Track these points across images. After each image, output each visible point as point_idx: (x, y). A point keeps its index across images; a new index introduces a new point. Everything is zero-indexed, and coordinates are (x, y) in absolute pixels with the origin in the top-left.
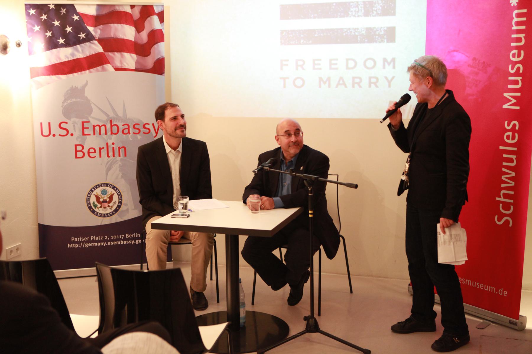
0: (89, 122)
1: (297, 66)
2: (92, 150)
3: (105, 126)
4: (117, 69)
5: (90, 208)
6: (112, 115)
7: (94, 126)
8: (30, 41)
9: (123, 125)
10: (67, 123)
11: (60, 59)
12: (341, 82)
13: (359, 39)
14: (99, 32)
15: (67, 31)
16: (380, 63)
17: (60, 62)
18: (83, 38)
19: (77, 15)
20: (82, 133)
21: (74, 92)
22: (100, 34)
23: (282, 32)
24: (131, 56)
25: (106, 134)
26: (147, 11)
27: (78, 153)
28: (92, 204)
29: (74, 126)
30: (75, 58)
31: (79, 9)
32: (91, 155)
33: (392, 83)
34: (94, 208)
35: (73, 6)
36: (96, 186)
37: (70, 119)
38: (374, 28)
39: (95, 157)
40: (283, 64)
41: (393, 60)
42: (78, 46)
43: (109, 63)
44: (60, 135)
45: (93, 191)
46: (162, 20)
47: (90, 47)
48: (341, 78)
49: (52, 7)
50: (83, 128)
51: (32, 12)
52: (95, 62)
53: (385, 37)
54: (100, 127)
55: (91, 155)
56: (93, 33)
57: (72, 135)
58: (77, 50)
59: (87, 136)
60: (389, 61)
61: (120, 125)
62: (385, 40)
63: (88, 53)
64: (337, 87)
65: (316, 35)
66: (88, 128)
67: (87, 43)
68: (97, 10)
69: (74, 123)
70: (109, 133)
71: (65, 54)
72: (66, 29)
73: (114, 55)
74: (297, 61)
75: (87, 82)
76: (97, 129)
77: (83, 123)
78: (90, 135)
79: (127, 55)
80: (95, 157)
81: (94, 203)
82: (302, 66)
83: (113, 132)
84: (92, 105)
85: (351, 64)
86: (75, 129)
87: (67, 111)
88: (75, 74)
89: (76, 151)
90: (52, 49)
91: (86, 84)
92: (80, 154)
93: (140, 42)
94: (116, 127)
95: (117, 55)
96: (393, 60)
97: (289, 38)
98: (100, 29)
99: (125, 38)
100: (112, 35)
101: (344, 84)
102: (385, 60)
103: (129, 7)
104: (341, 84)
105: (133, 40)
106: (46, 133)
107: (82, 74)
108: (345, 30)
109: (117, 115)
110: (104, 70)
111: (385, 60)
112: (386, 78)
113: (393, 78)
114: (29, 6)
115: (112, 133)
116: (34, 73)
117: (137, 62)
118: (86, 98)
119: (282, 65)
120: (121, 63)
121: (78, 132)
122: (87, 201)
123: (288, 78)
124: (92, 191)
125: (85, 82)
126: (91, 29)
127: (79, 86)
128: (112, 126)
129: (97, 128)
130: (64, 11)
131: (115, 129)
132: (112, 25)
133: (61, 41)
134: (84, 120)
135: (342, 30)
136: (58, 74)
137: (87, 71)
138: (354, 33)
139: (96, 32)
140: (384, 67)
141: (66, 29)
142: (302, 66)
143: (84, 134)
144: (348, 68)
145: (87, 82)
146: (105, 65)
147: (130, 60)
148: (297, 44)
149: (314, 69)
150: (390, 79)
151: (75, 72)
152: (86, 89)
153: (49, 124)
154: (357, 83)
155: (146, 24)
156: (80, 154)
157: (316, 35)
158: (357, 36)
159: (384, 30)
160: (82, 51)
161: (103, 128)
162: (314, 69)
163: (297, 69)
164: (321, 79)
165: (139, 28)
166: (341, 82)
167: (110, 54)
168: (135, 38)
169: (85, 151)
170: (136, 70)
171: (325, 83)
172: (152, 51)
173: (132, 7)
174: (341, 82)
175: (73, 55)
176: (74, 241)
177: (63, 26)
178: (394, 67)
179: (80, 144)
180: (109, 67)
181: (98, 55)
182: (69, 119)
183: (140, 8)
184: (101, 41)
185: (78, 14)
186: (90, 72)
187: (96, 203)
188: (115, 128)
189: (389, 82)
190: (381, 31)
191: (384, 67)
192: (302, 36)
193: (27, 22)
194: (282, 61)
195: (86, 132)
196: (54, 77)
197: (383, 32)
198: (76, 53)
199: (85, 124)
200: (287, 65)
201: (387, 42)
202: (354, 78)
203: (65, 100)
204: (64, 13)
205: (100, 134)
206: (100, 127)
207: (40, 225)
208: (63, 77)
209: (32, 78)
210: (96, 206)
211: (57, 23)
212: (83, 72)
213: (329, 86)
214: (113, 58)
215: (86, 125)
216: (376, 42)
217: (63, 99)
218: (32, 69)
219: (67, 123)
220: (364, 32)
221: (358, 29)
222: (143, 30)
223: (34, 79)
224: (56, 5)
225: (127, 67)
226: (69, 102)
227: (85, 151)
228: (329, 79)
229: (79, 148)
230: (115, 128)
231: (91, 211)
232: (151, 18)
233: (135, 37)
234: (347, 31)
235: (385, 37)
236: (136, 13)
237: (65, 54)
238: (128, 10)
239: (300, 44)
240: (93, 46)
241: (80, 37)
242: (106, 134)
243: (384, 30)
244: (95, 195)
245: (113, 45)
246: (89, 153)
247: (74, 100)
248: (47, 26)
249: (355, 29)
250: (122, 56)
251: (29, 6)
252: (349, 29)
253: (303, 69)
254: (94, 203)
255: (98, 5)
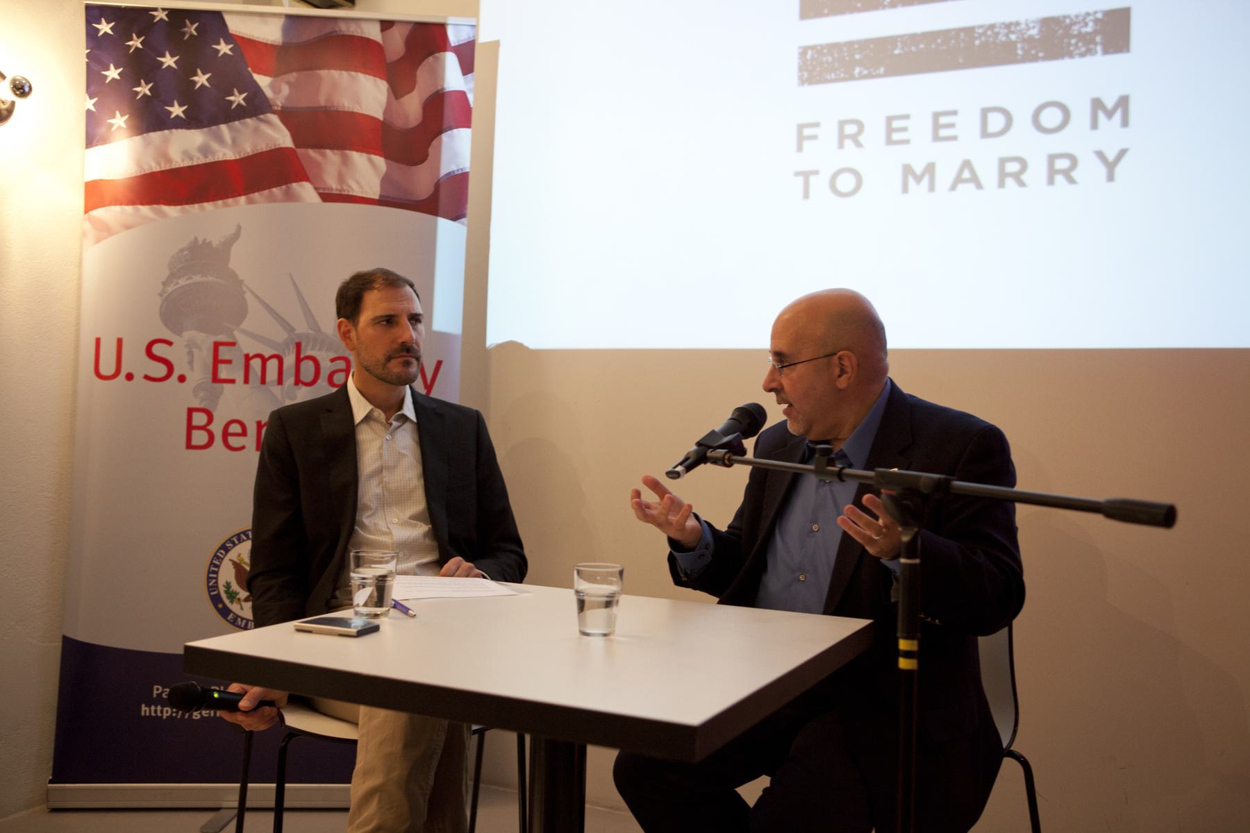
0: (233, 344)
1: (842, 137)
2: (235, 428)
3: (280, 359)
4: (327, 197)
5: (216, 600)
6: (301, 328)
7: (248, 358)
8: (93, 109)
9: (333, 360)
10: (170, 343)
11: (169, 160)
12: (966, 174)
13: (1020, 52)
14: (285, 90)
15: (195, 83)
16: (1081, 114)
17: (168, 168)
18: (239, 105)
19: (227, 43)
20: (210, 376)
21: (198, 256)
22: (288, 98)
23: (804, 51)
24: (370, 161)
25: (280, 381)
26: (427, 39)
27: (195, 433)
28: (222, 589)
29: (191, 353)
30: (210, 159)
31: (235, 25)
32: (233, 441)
33: (1119, 170)
34: (227, 601)
35: (218, 16)
36: (238, 535)
37: (179, 333)
38: (1065, 17)
39: (243, 447)
40: (804, 134)
41: (1123, 102)
42: (224, 128)
43: (308, 180)
44: (147, 377)
45: (227, 550)
46: (467, 67)
47: (256, 131)
48: (967, 164)
49: (161, 15)
50: (217, 361)
51: (105, 28)
52: (265, 174)
53: (1098, 39)
54: (264, 361)
55: (233, 441)
56: (269, 93)
57: (182, 379)
58: (220, 139)
59: (225, 385)
60: (1110, 104)
61: (324, 358)
62: (1099, 48)
63: (248, 148)
64: (953, 188)
65: (897, 52)
66: (229, 362)
67: (248, 120)
68: (286, 30)
69: (191, 346)
70: (289, 380)
71: (185, 147)
72: (195, 78)
73: (324, 156)
74: (842, 124)
75: (239, 228)
76: (255, 367)
77: (217, 345)
78: (233, 381)
79: (359, 159)
80: (243, 447)
81: (228, 585)
82: (855, 138)
83: (302, 378)
84: (248, 296)
85: (996, 122)
86: (191, 362)
87: (175, 310)
88: (208, 206)
89: (190, 428)
90: (148, 131)
91: (236, 236)
92: (199, 437)
93: (399, 123)
94: (311, 363)
95: (332, 156)
96: (1123, 102)
97: (820, 66)
98: (288, 83)
99: (357, 109)
100: (322, 101)
101: (975, 180)
102: (1097, 104)
103: (377, 27)
104: (966, 181)
105: (381, 117)
106: (107, 367)
107: (226, 205)
108: (981, 31)
109: (318, 330)
110: (290, 197)
111: (1097, 104)
112: (1100, 155)
113: (1122, 153)
114: (94, 14)
115: (298, 381)
116: (95, 194)
117: (386, 180)
118: (233, 275)
119: (801, 138)
120: (341, 179)
121: (198, 374)
122: (209, 579)
123: (816, 173)
124: (225, 548)
125: (232, 231)
126: (263, 81)
127: (216, 239)
128: (299, 360)
129: (256, 364)
130: (192, 29)
131: (307, 369)
132: (323, 73)
133: (177, 110)
134: (222, 338)
135: (969, 31)
136: (158, 203)
137: (243, 199)
138: (1007, 35)
139: (276, 90)
140: (1094, 125)
141: (195, 78)
142: (855, 138)
143: (216, 379)
144: (985, 134)
145: (239, 228)
146: (294, 185)
147: (366, 171)
148: (844, 80)
149: (890, 142)
150: (1111, 156)
151: (208, 201)
152: (235, 249)
153: (120, 341)
154: (1010, 175)
155: (422, 74)
156: (199, 437)
157: (897, 52)
158: (1015, 43)
159: (1096, 21)
160: (234, 141)
161: (272, 365)
162: (890, 142)
163: (841, 146)
164: (907, 170)
165: (398, 89)
166: (967, 174)
167: (312, 153)
168: (385, 113)
169: (217, 428)
170: (383, 202)
171: (918, 179)
172: (431, 150)
173: (386, 25)
174: (966, 174)
175: (204, 150)
176: (159, 695)
177: (187, 69)
178: (1125, 123)
179: (202, 406)
180: (306, 190)
181: (278, 154)
182: (178, 331)
183: (406, 30)
184: (287, 116)
185: (230, 38)
186: (251, 202)
187: (235, 587)
188: (308, 367)
189: (1111, 167)
190: (1086, 25)
191: (1094, 125)
192: (857, 57)
193: (88, 56)
194: (801, 127)
195: (224, 372)
196: (145, 210)
197: (1091, 24)
198: (215, 146)
199: (221, 348)
200: (814, 137)
201: (1106, 51)
202: (1003, 162)
203: (173, 276)
204: (192, 35)
205: (263, 381)
206: (264, 361)
207: (66, 640)
208: (172, 211)
209: (86, 211)
210: (232, 596)
211: (169, 61)
212: (230, 200)
213: (932, 188)
214: (318, 166)
215: (224, 353)
216: (1071, 55)
217: (167, 273)
218: (89, 8)
219: (170, 343)
220: (1034, 32)
221: (1017, 24)
222: (413, 89)
223: (91, 213)
224: (173, 13)
225: (357, 192)
226: (182, 282)
227: (217, 428)
228: (930, 169)
229: (200, 419)
230: (308, 367)
231: (219, 611)
232: (437, 59)
233: (386, 112)
234: (984, 34)
235: (1098, 39)
236: (396, 44)
237: (185, 147)
238: (374, 33)
239: (852, 78)
240: (265, 128)
241: (231, 102)
242: (280, 381)
243: (1096, 21)
244: (235, 563)
245: (324, 129)
246: (226, 434)
247: (197, 278)
248: (141, 66)
249: (1008, 26)
250: (346, 161)
251: (97, 12)
252: (992, 27)
253: (859, 145)
254: (228, 585)
255: (290, 17)
